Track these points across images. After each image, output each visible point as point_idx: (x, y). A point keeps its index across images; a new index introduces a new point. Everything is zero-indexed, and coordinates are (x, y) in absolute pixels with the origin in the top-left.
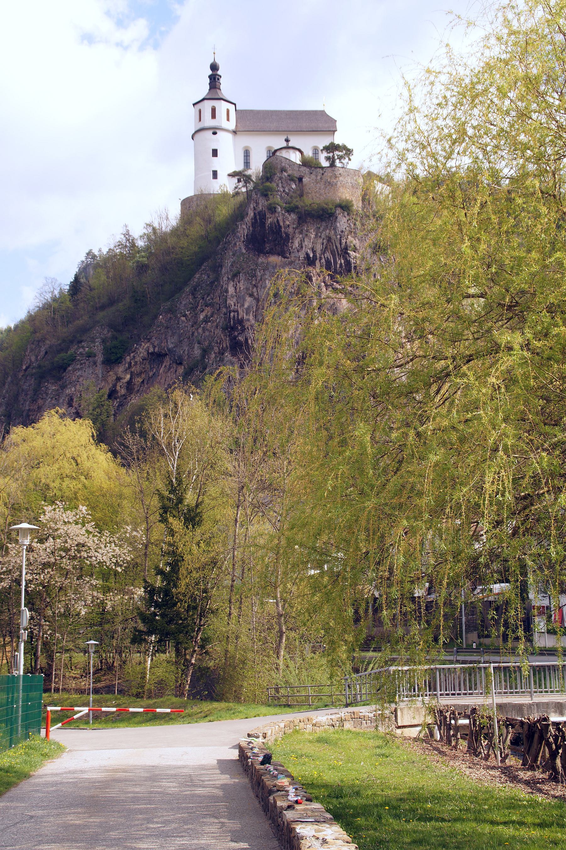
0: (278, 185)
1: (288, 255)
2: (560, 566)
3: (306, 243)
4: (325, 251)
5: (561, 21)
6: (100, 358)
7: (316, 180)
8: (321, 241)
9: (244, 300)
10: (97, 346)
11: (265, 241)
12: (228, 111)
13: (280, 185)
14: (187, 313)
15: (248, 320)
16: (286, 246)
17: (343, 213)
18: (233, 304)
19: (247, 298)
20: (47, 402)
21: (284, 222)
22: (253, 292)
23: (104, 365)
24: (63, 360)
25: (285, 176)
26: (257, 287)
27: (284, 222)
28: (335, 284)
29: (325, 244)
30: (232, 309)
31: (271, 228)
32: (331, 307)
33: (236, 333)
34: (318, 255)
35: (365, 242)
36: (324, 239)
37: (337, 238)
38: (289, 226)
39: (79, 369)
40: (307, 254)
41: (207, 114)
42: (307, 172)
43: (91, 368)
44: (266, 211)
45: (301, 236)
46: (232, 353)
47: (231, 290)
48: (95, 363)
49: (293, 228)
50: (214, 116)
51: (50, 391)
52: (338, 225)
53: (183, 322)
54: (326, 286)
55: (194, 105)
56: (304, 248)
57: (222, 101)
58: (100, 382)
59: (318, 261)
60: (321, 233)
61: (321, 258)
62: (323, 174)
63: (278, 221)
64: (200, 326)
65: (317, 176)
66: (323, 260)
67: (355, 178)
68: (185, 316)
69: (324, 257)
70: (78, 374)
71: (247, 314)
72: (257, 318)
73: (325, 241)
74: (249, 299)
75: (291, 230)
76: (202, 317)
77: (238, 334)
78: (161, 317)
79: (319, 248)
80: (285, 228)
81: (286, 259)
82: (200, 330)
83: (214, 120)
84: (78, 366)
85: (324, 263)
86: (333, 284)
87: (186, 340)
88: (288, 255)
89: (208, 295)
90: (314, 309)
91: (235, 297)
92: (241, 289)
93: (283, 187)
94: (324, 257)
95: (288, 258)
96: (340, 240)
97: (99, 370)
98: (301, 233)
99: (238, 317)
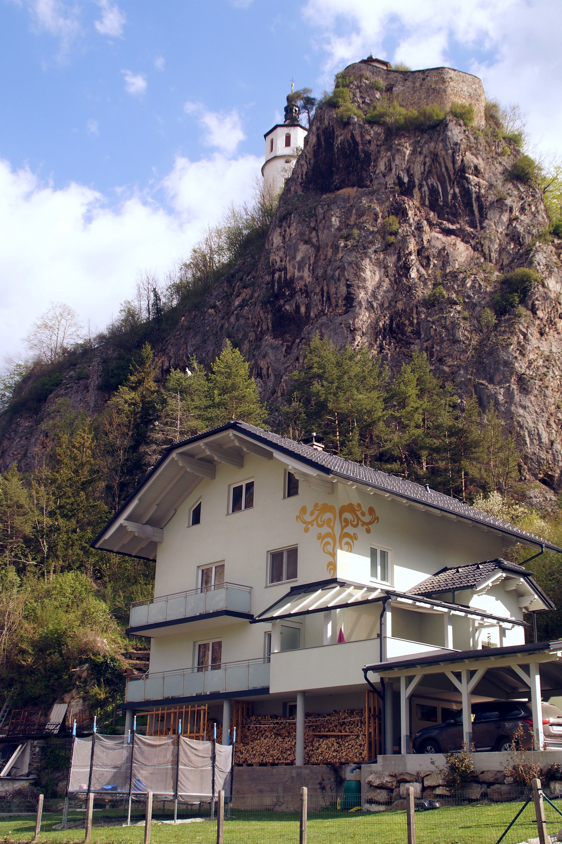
1: (369, 183)
3: (397, 162)
4: (427, 176)
5: (559, 415)
6: (94, 382)
7: (413, 88)
8: (422, 158)
9: (296, 250)
10: (94, 366)
11: (332, 172)
15: (302, 278)
16: (366, 171)
18: (278, 259)
19: (300, 247)
20: (15, 443)
21: (362, 136)
22: (310, 239)
23: (100, 392)
24: (44, 385)
26: (317, 231)
27: (362, 136)
28: (445, 222)
29: (428, 164)
30: (276, 267)
31: (342, 149)
32: (440, 252)
33: (282, 302)
34: (417, 181)
35: (492, 166)
36: (426, 157)
37: (447, 154)
38: (369, 142)
39: (62, 395)
40: (399, 178)
41: (280, 142)
42: (399, 79)
43: (80, 394)
44: (335, 125)
45: (389, 154)
46: (274, 335)
48: (87, 388)
49: (377, 145)
51: (21, 429)
53: (210, 315)
54: (430, 224)
55: (266, 136)
56: (394, 170)
57: (299, 128)
58: (90, 413)
59: (416, 190)
60: (422, 148)
61: (421, 186)
62: (424, 79)
63: (353, 136)
64: (233, 313)
65: (414, 83)
66: (425, 188)
67: (474, 87)
68: (214, 307)
70: (59, 402)
71: (299, 270)
72: (316, 274)
73: (427, 159)
74: (303, 248)
75: (373, 147)
76: (237, 303)
77: (285, 302)
78: (183, 318)
79: (418, 170)
80: (364, 144)
81: (364, 189)
82: (232, 319)
83: (288, 148)
84: (62, 392)
85: (427, 193)
86: (441, 223)
87: (211, 338)
89: (249, 274)
90: (410, 254)
91: (283, 250)
95: (368, 187)
96: (453, 157)
97: (92, 397)
98: (389, 149)
99: (285, 277)
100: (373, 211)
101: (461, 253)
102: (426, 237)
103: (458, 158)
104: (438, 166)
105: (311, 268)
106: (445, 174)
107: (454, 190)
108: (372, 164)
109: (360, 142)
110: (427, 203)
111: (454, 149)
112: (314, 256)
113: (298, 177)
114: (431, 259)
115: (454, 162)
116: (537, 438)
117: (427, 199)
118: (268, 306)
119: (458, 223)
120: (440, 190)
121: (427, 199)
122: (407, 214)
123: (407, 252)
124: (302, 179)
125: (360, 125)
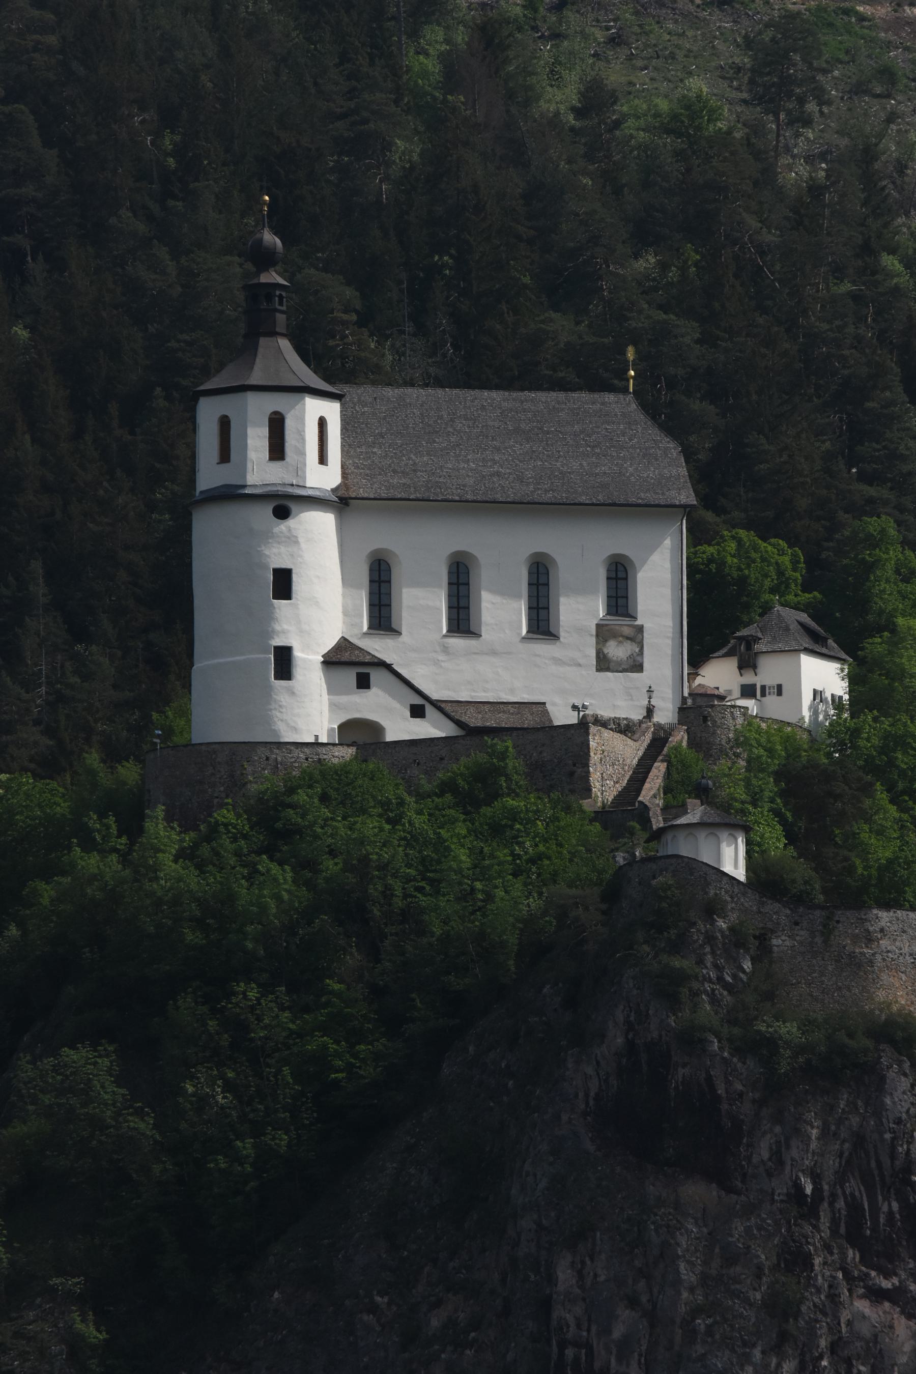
0: (700, 962)
1: (739, 1184)
2: (106, 1093)
12: (322, 423)
13: (709, 959)
14: (378, 1299)
17: (900, 1063)
25: (721, 931)
34: (826, 1187)
36: (844, 1141)
38: (741, 1095)
45: (778, 1129)
47: (565, 1276)
50: (277, 451)
52: (888, 1101)
56: (788, 1168)
61: (833, 1197)
63: (709, 1079)
66: (841, 1204)
69: (844, 1193)
73: (847, 1145)
81: (734, 1197)
83: (277, 465)
86: (867, 1275)
88: (739, 1184)
90: (821, 1357)
92: (602, 1278)
93: (716, 966)
94: (844, 1193)
95: (738, 1193)
96: (893, 1148)
100: (755, 1261)
101: (903, 1343)
102: (845, 1316)
103: (900, 1149)
104: (863, 1155)
105: (643, 1360)
106: (876, 1172)
107: (890, 1205)
108: (745, 1141)
109: (724, 1095)
110: (843, 1230)
111: (894, 1132)
112: (647, 1337)
113: (576, 1096)
114: (854, 1362)
115: (893, 1156)
116: (781, 138)
117: (843, 1225)
118: (170, 923)
119: (896, 1275)
120: (866, 1207)
121: (843, 1225)
122: (813, 1265)
123: (817, 1355)
124: (587, 1104)
125: (724, 1058)
